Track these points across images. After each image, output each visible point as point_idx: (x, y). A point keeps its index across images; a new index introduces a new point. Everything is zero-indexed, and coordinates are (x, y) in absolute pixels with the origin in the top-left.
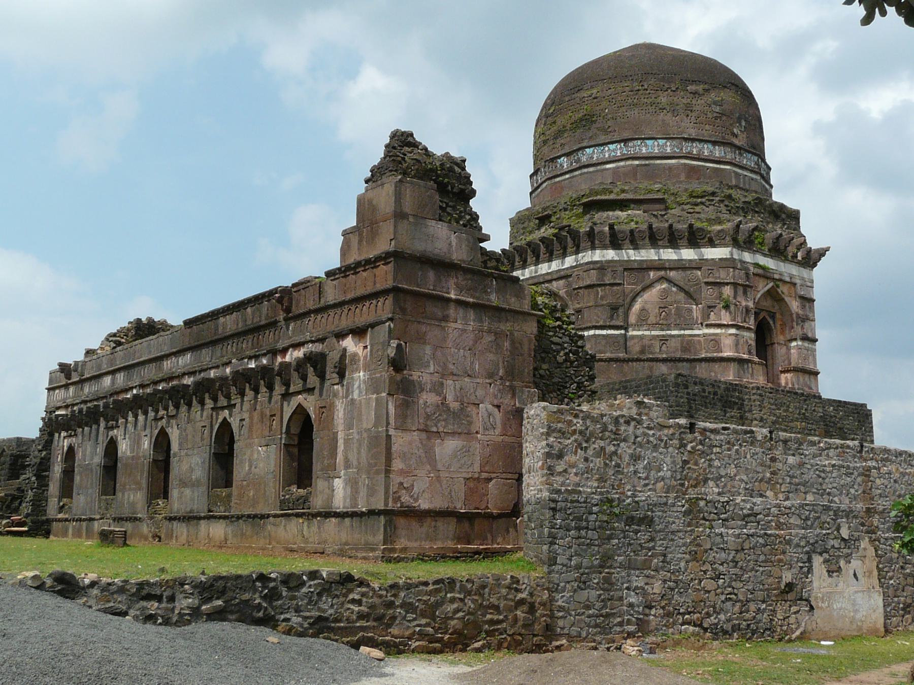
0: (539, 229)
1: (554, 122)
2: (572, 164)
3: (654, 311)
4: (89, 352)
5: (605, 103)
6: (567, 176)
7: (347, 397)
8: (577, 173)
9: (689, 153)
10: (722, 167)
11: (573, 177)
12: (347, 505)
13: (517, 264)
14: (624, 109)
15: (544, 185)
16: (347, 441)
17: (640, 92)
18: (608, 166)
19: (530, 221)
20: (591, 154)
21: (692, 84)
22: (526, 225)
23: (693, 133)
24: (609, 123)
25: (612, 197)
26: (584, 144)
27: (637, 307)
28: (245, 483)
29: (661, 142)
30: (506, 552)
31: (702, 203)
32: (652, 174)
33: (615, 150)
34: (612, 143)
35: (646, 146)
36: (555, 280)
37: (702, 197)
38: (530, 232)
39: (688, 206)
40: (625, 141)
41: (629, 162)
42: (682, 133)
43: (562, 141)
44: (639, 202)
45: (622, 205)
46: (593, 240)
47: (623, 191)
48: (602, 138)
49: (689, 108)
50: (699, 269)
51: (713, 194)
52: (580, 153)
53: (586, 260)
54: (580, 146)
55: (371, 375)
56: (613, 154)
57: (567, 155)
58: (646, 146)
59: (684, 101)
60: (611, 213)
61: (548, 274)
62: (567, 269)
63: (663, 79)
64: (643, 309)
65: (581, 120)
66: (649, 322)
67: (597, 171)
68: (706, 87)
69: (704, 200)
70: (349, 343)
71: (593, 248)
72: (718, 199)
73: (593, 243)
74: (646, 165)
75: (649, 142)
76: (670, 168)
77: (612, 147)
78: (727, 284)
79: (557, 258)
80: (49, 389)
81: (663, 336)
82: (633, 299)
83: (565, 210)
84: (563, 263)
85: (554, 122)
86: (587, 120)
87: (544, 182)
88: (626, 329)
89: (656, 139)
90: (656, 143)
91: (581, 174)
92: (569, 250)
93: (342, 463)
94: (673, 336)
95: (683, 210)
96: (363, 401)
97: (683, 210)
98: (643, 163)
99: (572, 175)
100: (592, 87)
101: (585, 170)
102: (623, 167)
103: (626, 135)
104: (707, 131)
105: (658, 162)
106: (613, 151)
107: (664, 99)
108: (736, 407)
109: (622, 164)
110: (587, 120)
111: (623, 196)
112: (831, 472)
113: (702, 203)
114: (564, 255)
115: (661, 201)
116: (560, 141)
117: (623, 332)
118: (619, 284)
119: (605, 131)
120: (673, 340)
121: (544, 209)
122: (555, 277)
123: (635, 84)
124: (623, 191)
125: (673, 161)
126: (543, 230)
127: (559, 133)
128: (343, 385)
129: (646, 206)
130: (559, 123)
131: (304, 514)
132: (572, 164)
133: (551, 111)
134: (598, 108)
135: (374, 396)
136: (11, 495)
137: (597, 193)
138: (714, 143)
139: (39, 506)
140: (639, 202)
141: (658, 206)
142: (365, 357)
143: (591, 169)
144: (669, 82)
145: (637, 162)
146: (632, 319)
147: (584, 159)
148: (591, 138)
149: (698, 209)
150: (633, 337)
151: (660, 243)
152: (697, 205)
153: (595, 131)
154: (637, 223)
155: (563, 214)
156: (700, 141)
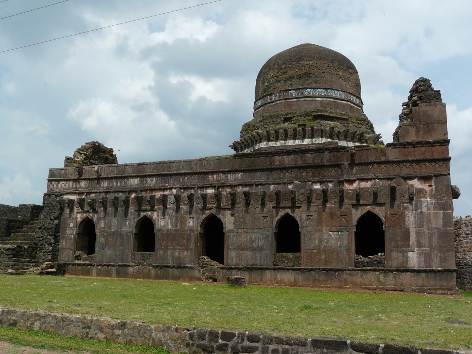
0: (284, 122)
1: (286, 73)
2: (298, 94)
4: (68, 160)
5: (316, 70)
6: (295, 100)
7: (416, 210)
8: (301, 99)
11: (299, 101)
12: (421, 266)
13: (271, 138)
14: (325, 74)
15: (279, 102)
16: (419, 234)
17: (332, 68)
18: (318, 99)
19: (277, 118)
20: (308, 92)
22: (275, 120)
23: (350, 90)
24: (318, 79)
25: (327, 114)
26: (306, 86)
28: (315, 251)
29: (341, 92)
30: (328, 287)
31: (361, 124)
32: (337, 106)
33: (321, 92)
34: (320, 88)
35: (335, 93)
36: (112, 192)
37: (361, 121)
38: (278, 124)
39: (356, 124)
40: (327, 89)
43: (292, 83)
44: (338, 119)
45: (331, 119)
46: (322, 134)
47: (331, 112)
48: (315, 86)
49: (349, 79)
52: (303, 91)
53: (317, 142)
54: (304, 87)
55: (437, 200)
56: (320, 94)
57: (295, 90)
58: (335, 93)
60: (327, 122)
61: (292, 145)
62: (305, 145)
63: (340, 64)
65: (303, 74)
67: (312, 100)
69: (361, 122)
70: (416, 183)
71: (322, 137)
72: (366, 122)
74: (335, 102)
75: (336, 92)
76: (344, 105)
77: (320, 90)
79: (299, 138)
80: (49, 181)
83: (301, 116)
84: (303, 142)
85: (286, 73)
86: (307, 76)
87: (280, 100)
89: (339, 91)
91: (304, 100)
92: (307, 136)
93: (415, 244)
95: (354, 125)
96: (431, 213)
97: (354, 125)
99: (298, 100)
100: (309, 60)
101: (307, 99)
102: (325, 101)
103: (326, 86)
105: (339, 101)
106: (321, 92)
107: (341, 73)
109: (325, 99)
110: (307, 76)
111: (331, 115)
113: (361, 124)
114: (304, 137)
115: (347, 120)
116: (289, 83)
119: (316, 82)
121: (288, 114)
123: (329, 64)
124: (331, 112)
125: (345, 102)
126: (286, 124)
127: (291, 78)
128: (412, 204)
129: (341, 121)
130: (289, 73)
131: (382, 270)
132: (298, 94)
133: (284, 67)
134: (313, 71)
135: (442, 212)
136: (31, 247)
137: (321, 111)
139: (55, 255)
140: (338, 119)
141: (345, 122)
142: (431, 191)
143: (310, 99)
144: (343, 66)
145: (331, 100)
147: (306, 93)
148: (309, 84)
149: (360, 126)
151: (348, 139)
152: (359, 124)
153: (311, 81)
154: (338, 128)
155: (299, 118)
156: (353, 95)
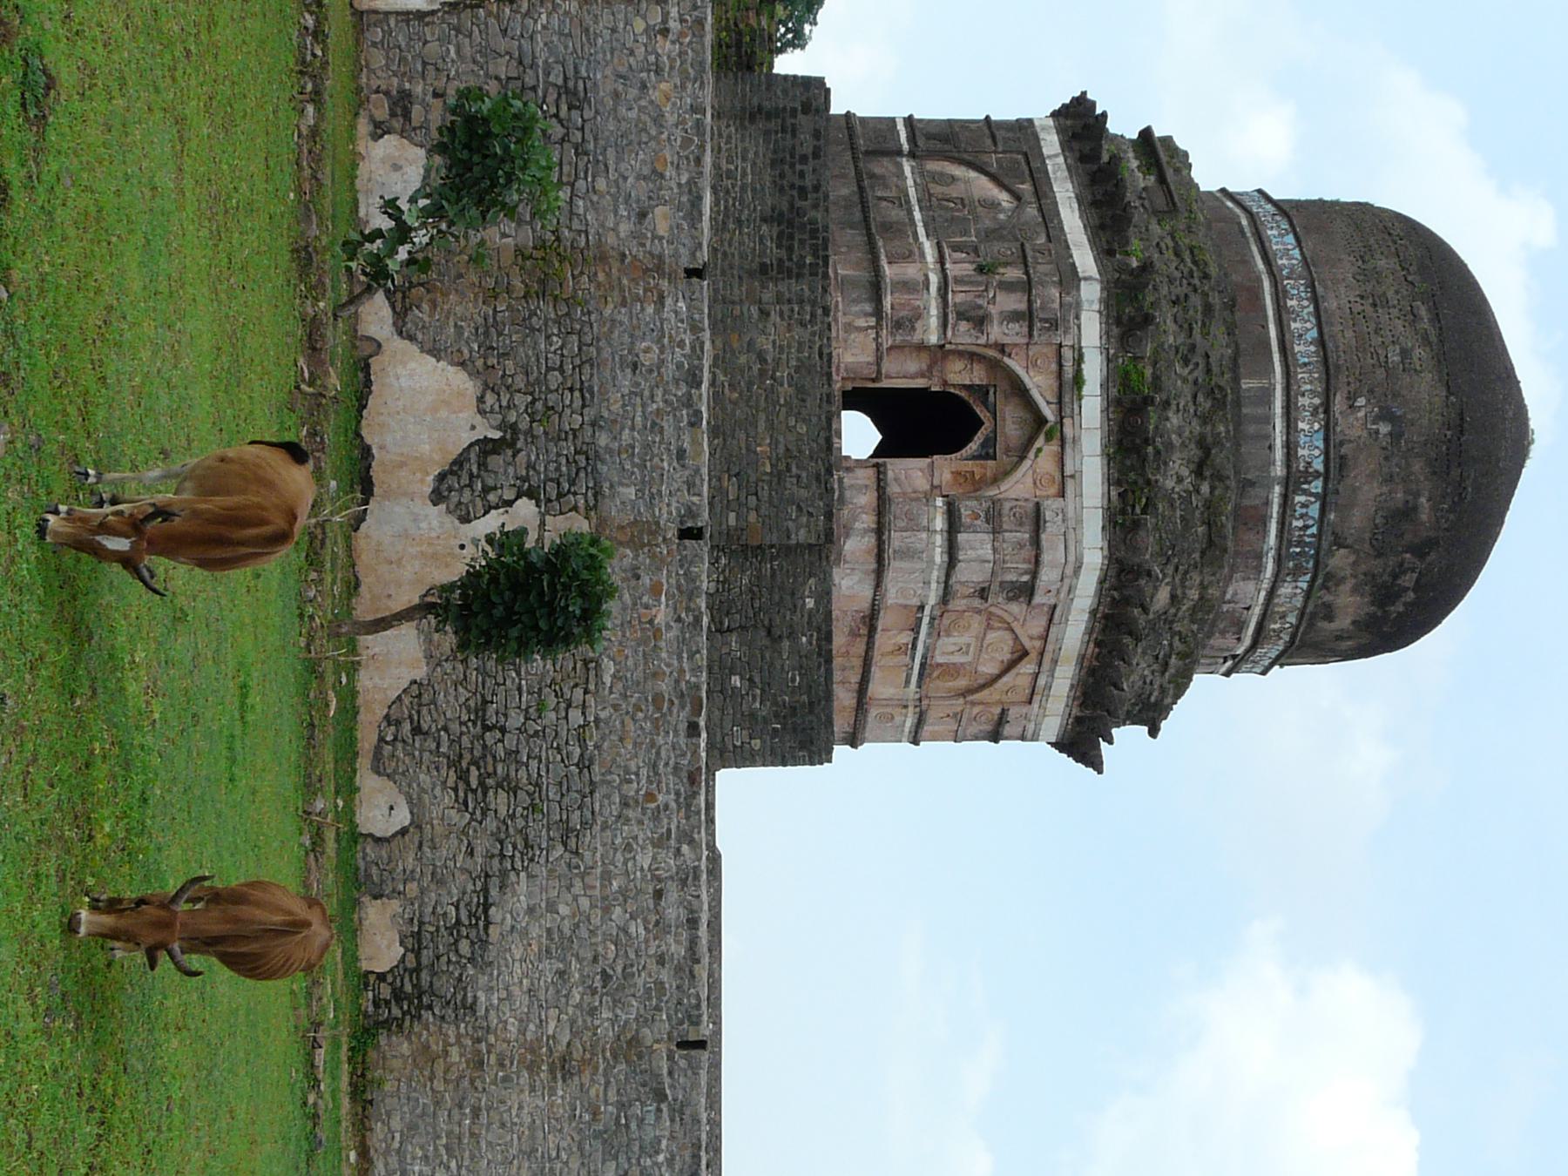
3: (953, 191)
9: (1285, 292)
10: (1276, 357)
21: (1429, 310)
23: (1331, 304)
27: (958, 171)
41: (1238, 211)
42: (1322, 282)
50: (1049, 239)
51: (1206, 276)
59: (1390, 294)
64: (954, 179)
66: (931, 185)
68: (1433, 339)
73: (701, 1045)
78: (1027, 273)
81: (908, 202)
82: (971, 165)
88: (912, 155)
90: (1317, 452)
94: (910, 212)
98: (1247, 230)
104: (1344, 338)
105: (1254, 248)
108: (783, 254)
112: (660, 927)
117: (906, 147)
118: (995, 144)
120: (903, 213)
122: (1042, 681)
125: (1261, 266)
138: (1321, 342)
146: (933, 166)
150: (900, 167)
152: (1177, 254)
